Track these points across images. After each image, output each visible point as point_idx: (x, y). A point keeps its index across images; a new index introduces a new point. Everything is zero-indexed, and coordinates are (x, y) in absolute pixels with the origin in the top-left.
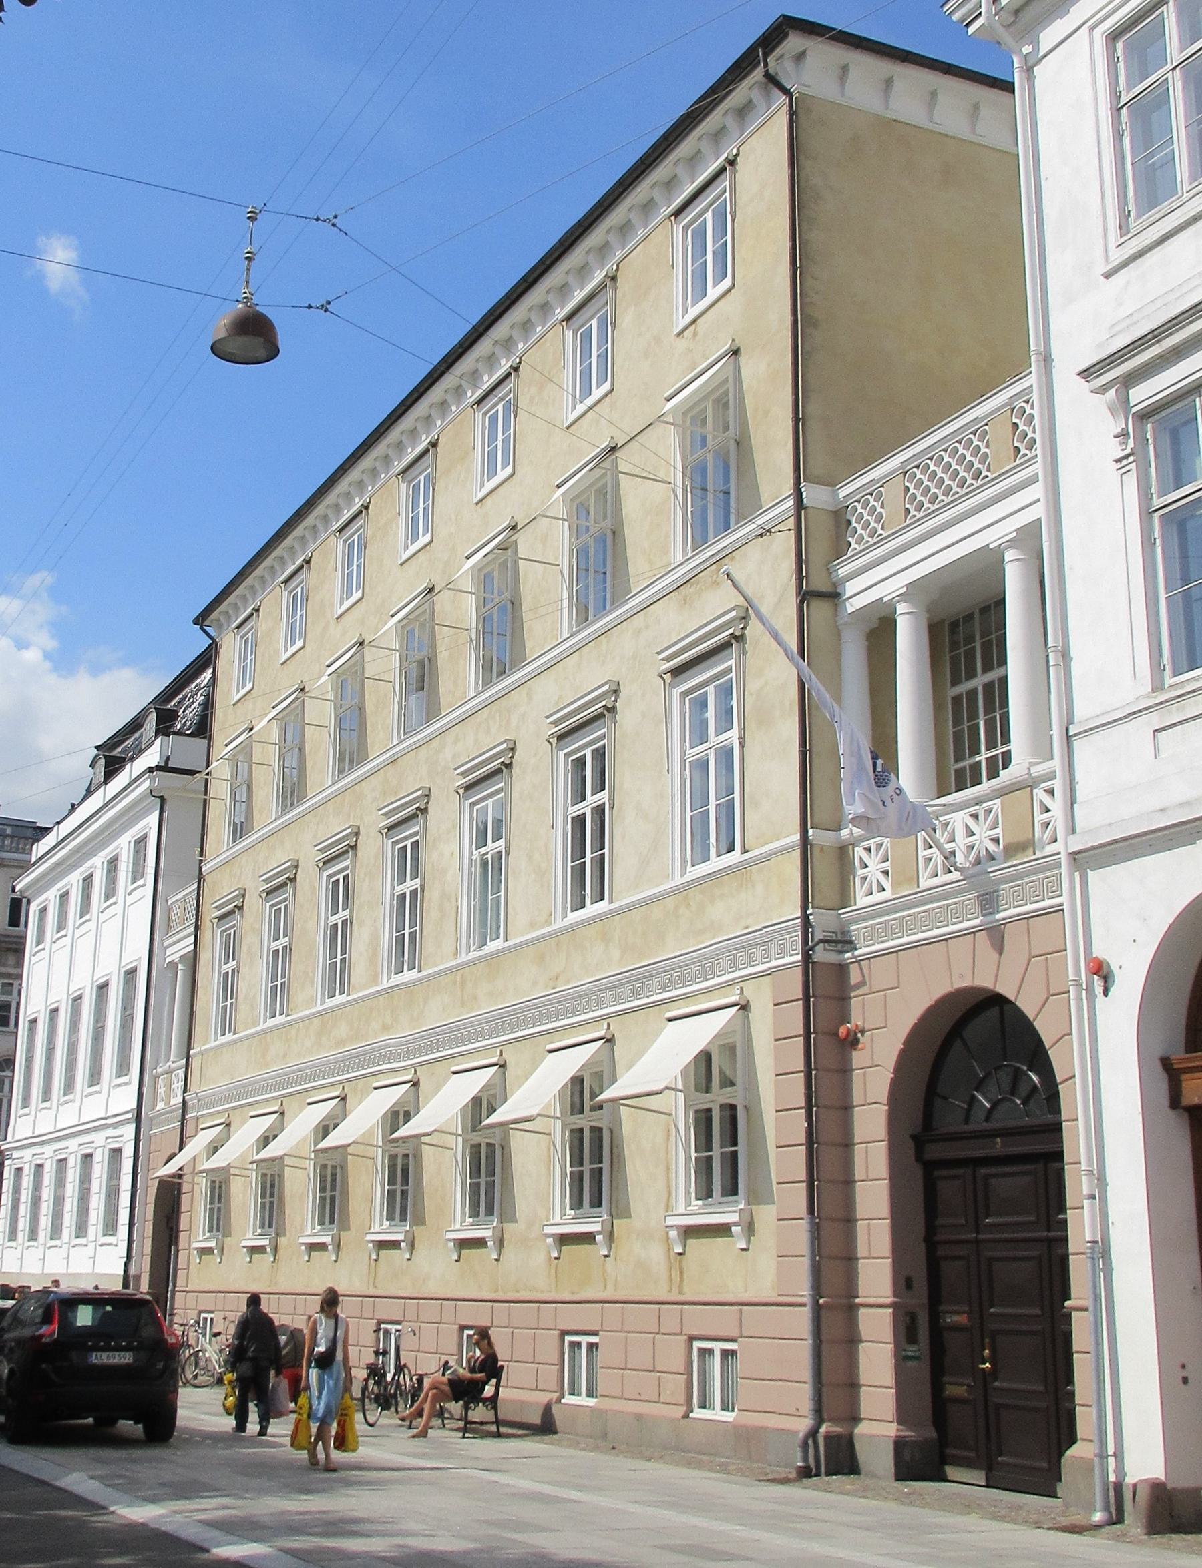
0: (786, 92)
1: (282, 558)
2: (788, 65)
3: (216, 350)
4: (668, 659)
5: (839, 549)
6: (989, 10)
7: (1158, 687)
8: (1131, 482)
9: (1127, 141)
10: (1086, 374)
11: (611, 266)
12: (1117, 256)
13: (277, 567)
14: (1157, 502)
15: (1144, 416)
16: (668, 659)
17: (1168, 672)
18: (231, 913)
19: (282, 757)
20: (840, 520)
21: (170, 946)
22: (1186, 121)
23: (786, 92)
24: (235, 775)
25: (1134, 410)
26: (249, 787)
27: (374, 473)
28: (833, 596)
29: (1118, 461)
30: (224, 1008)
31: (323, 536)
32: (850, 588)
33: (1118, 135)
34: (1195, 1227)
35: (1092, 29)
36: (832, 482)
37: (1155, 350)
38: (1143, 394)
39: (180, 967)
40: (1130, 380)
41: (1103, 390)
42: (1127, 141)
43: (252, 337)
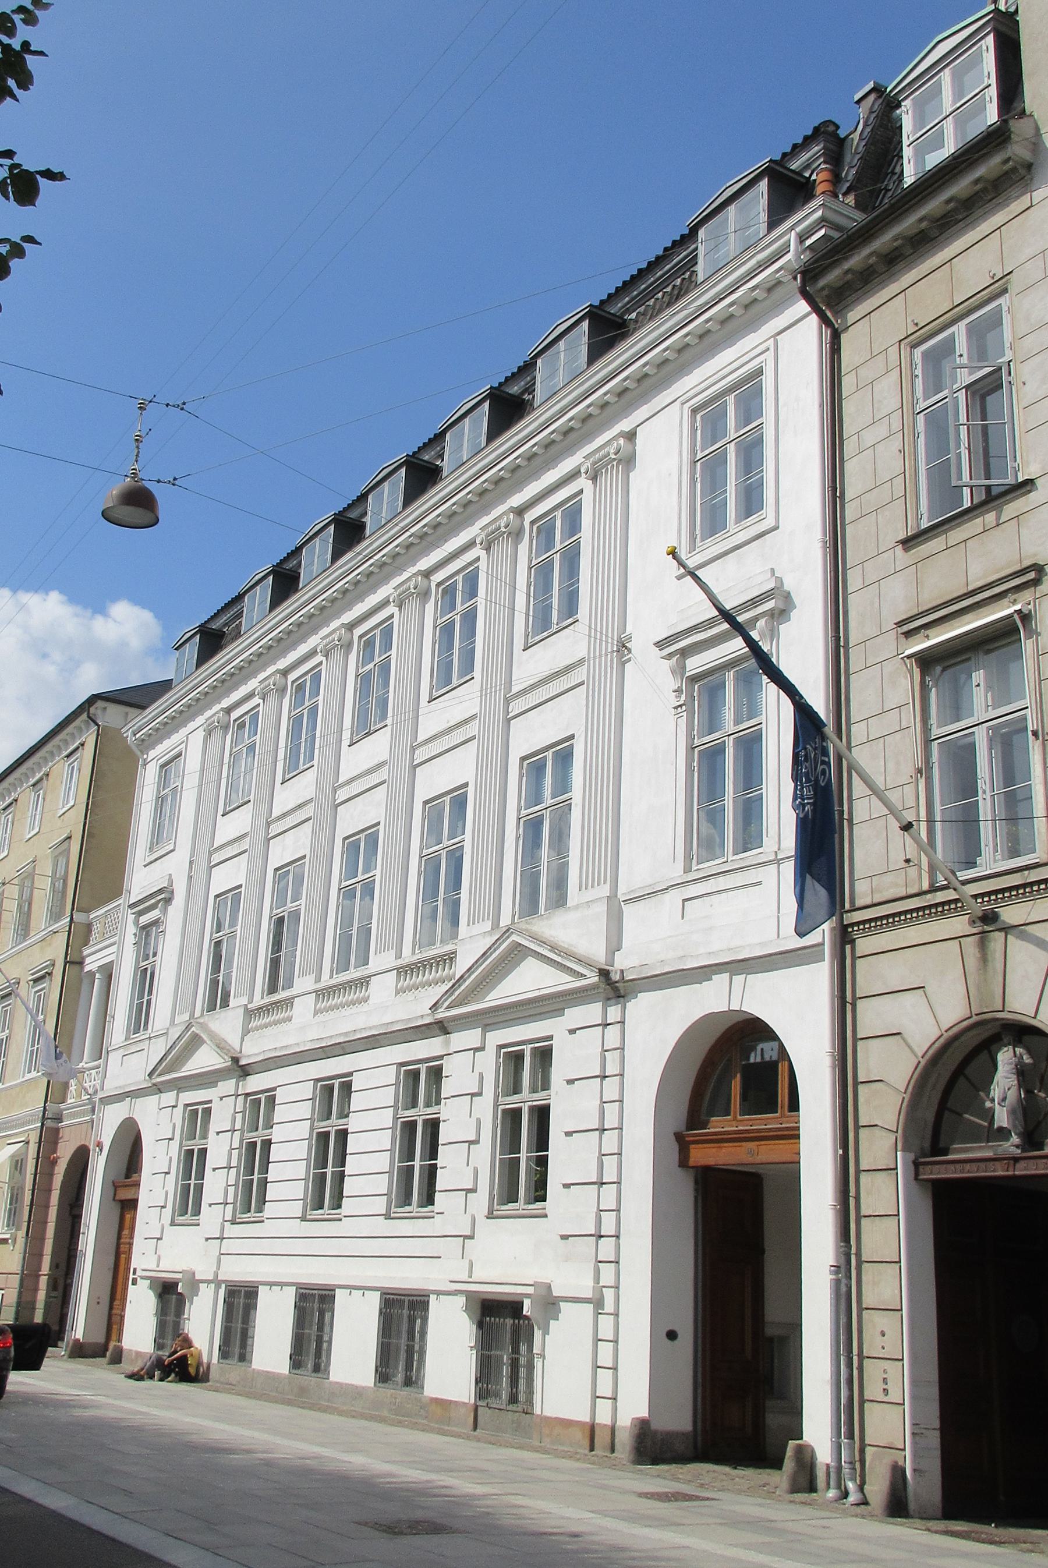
0: (97, 724)
1: (26, 774)
2: (99, 712)
3: (106, 515)
4: (33, 974)
5: (86, 943)
6: (796, 250)
7: (687, 870)
8: (683, 722)
9: (698, 485)
10: (660, 645)
11: (14, 796)
12: (148, 860)
13: (49, 758)
14: (696, 742)
15: (694, 679)
16: (33, 974)
17: (694, 861)
18: (43, 977)
19: (53, 884)
20: (89, 927)
21: (89, 955)
22: (736, 480)
23: (97, 724)
24: (21, 895)
25: (688, 674)
26: (30, 904)
27: (52, 754)
28: (81, 963)
29: (676, 708)
30: (32, 1051)
31: (57, 758)
32: (88, 960)
33: (693, 481)
34: (933, 1267)
35: (683, 404)
36: (88, 911)
37: (147, 904)
38: (696, 664)
39: (97, 976)
40: (685, 653)
41: (670, 656)
42: (698, 485)
43: (138, 504)
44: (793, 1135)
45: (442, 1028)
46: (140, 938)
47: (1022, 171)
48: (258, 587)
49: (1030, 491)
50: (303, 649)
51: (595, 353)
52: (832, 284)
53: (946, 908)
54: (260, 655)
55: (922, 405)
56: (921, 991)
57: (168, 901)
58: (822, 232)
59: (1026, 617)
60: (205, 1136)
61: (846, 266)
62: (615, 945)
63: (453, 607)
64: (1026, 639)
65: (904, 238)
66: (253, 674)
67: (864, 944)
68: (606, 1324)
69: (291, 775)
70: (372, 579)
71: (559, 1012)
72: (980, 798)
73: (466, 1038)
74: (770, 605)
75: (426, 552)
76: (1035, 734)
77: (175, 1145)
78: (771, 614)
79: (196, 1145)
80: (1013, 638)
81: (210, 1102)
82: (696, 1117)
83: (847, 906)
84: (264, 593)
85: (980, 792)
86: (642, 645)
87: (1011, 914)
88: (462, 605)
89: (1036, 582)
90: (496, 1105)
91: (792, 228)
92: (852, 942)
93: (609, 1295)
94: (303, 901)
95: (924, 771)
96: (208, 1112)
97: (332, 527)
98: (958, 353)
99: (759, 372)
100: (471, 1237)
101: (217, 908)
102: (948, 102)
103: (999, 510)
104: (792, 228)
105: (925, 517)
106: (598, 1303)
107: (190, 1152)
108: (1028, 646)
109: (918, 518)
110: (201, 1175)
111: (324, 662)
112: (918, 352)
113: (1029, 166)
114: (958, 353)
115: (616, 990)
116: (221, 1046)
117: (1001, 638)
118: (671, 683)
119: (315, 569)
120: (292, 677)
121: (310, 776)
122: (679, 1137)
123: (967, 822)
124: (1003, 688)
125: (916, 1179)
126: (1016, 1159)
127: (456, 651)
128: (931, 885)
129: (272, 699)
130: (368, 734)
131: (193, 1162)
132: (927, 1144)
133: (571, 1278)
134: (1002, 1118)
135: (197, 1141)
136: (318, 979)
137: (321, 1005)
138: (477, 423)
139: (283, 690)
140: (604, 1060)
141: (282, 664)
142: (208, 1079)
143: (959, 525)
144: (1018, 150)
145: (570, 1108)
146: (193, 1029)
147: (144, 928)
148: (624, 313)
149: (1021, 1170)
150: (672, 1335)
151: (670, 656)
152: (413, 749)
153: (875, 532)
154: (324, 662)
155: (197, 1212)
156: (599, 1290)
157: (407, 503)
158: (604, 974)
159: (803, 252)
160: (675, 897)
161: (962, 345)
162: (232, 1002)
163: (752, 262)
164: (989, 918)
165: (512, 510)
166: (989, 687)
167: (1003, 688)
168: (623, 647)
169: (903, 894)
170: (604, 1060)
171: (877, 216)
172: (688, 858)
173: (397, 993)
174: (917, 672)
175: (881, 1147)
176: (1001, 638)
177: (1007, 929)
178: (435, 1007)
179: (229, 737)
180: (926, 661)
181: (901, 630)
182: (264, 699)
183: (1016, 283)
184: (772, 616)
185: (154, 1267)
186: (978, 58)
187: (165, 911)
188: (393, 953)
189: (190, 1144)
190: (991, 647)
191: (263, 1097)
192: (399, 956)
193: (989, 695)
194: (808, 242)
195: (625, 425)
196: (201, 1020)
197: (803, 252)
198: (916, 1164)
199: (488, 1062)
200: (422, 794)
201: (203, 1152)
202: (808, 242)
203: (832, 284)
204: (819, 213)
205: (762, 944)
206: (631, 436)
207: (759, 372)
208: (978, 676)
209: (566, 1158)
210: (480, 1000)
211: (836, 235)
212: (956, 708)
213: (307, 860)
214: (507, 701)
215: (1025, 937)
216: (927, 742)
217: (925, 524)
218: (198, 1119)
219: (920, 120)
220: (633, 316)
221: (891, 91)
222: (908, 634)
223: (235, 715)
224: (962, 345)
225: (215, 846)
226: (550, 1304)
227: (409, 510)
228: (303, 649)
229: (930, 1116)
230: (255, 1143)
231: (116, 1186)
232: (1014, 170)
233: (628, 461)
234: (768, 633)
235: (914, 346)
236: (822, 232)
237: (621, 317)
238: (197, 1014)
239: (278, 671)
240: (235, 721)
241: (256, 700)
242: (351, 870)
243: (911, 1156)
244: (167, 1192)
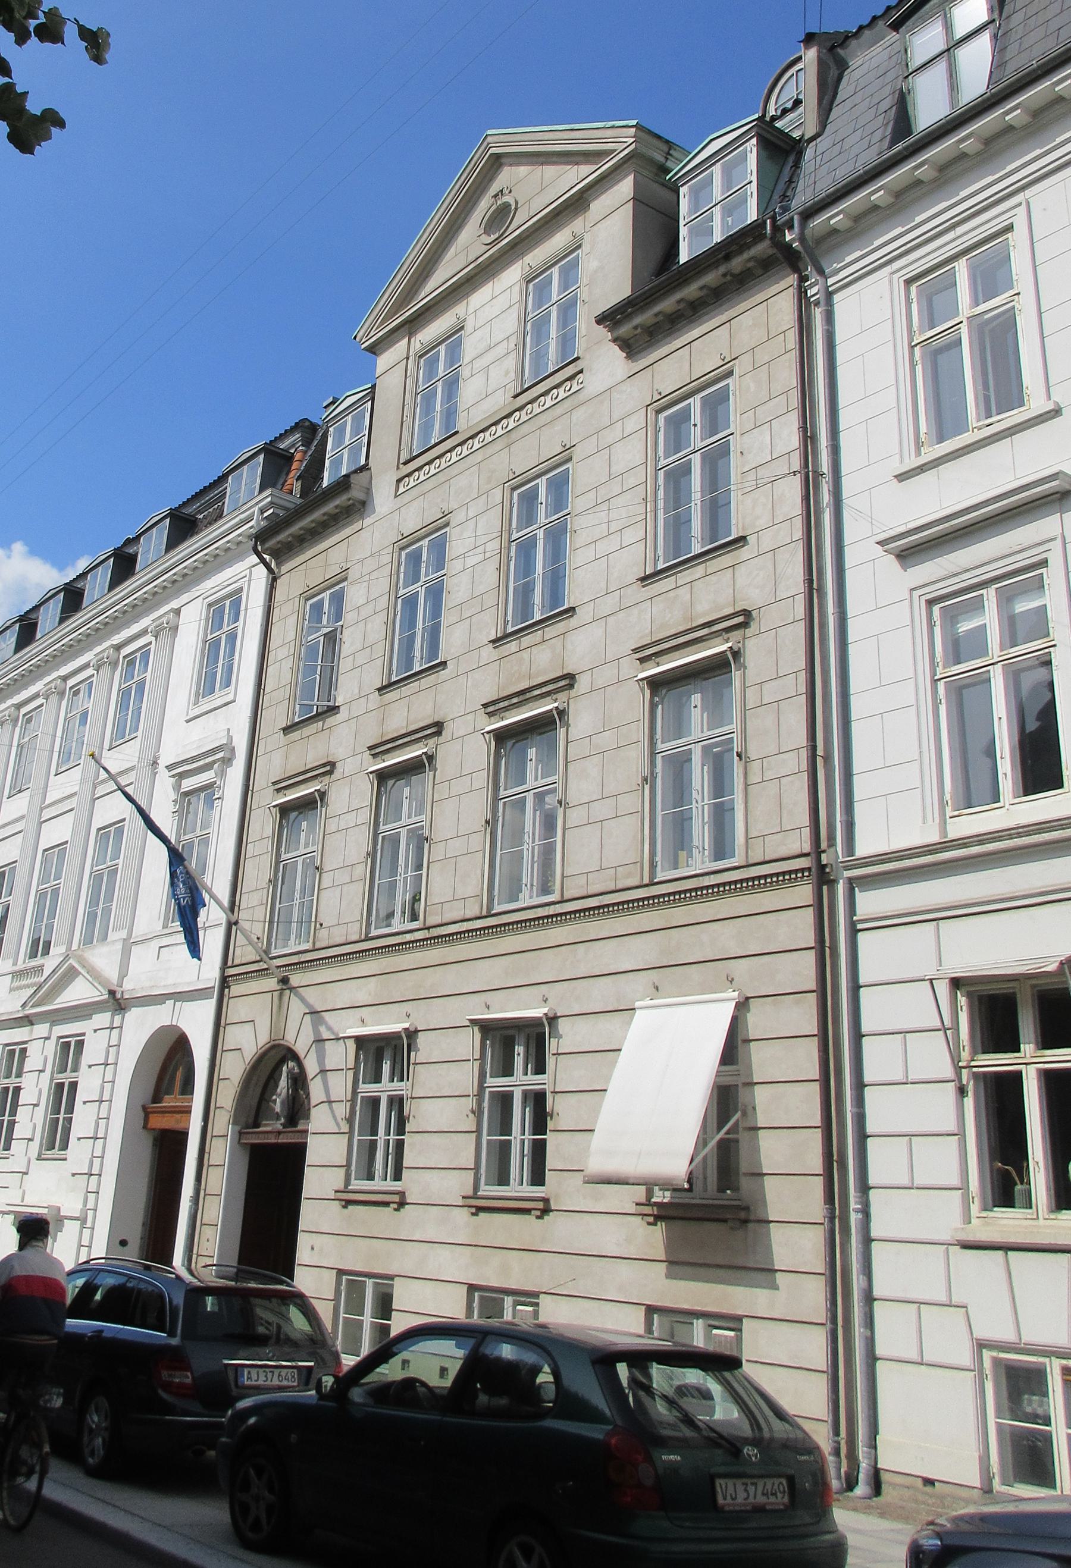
7: (165, 926)
12: (192, 715)
40: (182, 776)
44: (188, 1111)
45: (28, 1021)
46: (182, 806)
47: (359, 506)
48: (246, 467)
49: (743, 546)
50: (135, 628)
51: (172, 544)
52: (277, 541)
53: (787, 877)
54: (134, 606)
55: (515, 536)
56: (250, 1025)
57: (228, 761)
58: (271, 511)
59: (562, 713)
60: (75, 1069)
61: (657, 308)
62: (123, 974)
63: (221, 627)
64: (736, 670)
65: (342, 507)
66: (40, 677)
67: (236, 989)
68: (86, 1233)
69: (118, 743)
70: (147, 604)
71: (89, 1017)
72: (694, 806)
73: (41, 1029)
74: (221, 755)
75: (65, 662)
76: (739, 755)
77: (46, 1077)
78: (222, 760)
79: (66, 1078)
80: (725, 671)
81: (83, 1034)
82: (156, 1098)
83: (230, 963)
84: (160, 536)
85: (694, 802)
86: (163, 762)
87: (295, 980)
88: (228, 625)
89: (745, 625)
90: (52, 1080)
91: (257, 504)
92: (229, 987)
93: (90, 1213)
94: (121, 861)
95: (649, 779)
96: (80, 1044)
97: (168, 520)
98: (692, 423)
99: (241, 590)
100: (26, 1173)
101: (45, 861)
102: (717, 192)
103: (324, 720)
104: (257, 504)
105: (661, 559)
106: (83, 1220)
107: (60, 1086)
108: (736, 675)
109: (656, 561)
110: (70, 1109)
111: (154, 643)
112: (662, 417)
113: (363, 503)
114: (692, 423)
115: (119, 1004)
116: (96, 976)
117: (718, 668)
118: (173, 796)
119: (151, 557)
120: (24, 711)
121: (135, 745)
122: (144, 1108)
123: (681, 825)
124: (717, 711)
125: (239, 1142)
126: (279, 1133)
127: (220, 665)
128: (366, 935)
129: (54, 699)
130: (20, 791)
131: (64, 1096)
132: (251, 1121)
133: (71, 1206)
134: (278, 1108)
135: (68, 1073)
136: (15, 964)
137: (16, 984)
138: (253, 469)
139: (62, 694)
140: (108, 1053)
141: (64, 671)
142: (82, 1011)
143: (307, 725)
144: (356, 493)
145: (88, 1083)
146: (71, 961)
147: (187, 794)
148: (197, 514)
149: (282, 1140)
150: (123, 1243)
151: (173, 776)
152: (42, 810)
153: (275, 716)
154: (154, 643)
155: (65, 1146)
156: (85, 1211)
157: (111, 587)
158: (112, 993)
159: (263, 519)
160: (155, 944)
161: (696, 416)
162: (112, 936)
163: (237, 520)
164: (284, 981)
165: (113, 646)
166: (538, 761)
167: (717, 711)
168: (155, 763)
169: (613, 888)
170: (108, 1053)
171: (663, 282)
172: (166, 919)
173: (11, 990)
174: (647, 692)
175: (222, 1122)
176: (718, 668)
177: (292, 989)
178: (24, 1005)
179: (118, 673)
180: (656, 684)
181: (638, 656)
182: (156, 637)
183: (578, 454)
184: (223, 762)
185: (19, 1202)
186: (744, 157)
187: (222, 774)
188: (11, 961)
189: (60, 1078)
190: (543, 730)
191: (73, 1040)
192: (15, 964)
193: (705, 715)
194: (266, 514)
195: (174, 604)
196: (80, 953)
197: (263, 519)
198: (240, 1133)
199: (51, 1047)
200: (97, 823)
201: (74, 1086)
202: (266, 514)
203: (277, 541)
204: (269, 499)
205: (189, 984)
206: (177, 612)
207: (241, 590)
208: (696, 699)
209: (83, 1120)
210: (51, 1003)
211: (278, 511)
212: (679, 727)
213: (126, 823)
214: (95, 787)
215: (298, 995)
216: (653, 754)
217: (661, 566)
218: (70, 1052)
219: (695, 205)
220: (201, 517)
221: (670, 179)
222: (278, 790)
223: (71, 682)
224: (696, 416)
225: (47, 802)
226: (60, 1220)
227: (169, 556)
228: (135, 628)
229: (254, 1103)
230: (63, 1084)
231: (147, 1112)
232: (353, 505)
233: (175, 629)
234: (219, 773)
235: (658, 412)
236: (271, 511)
237: (193, 516)
238: (75, 947)
239: (60, 677)
240: (125, 657)
241: (90, 671)
242: (100, 858)
243: (238, 1128)
244: (35, 1125)
